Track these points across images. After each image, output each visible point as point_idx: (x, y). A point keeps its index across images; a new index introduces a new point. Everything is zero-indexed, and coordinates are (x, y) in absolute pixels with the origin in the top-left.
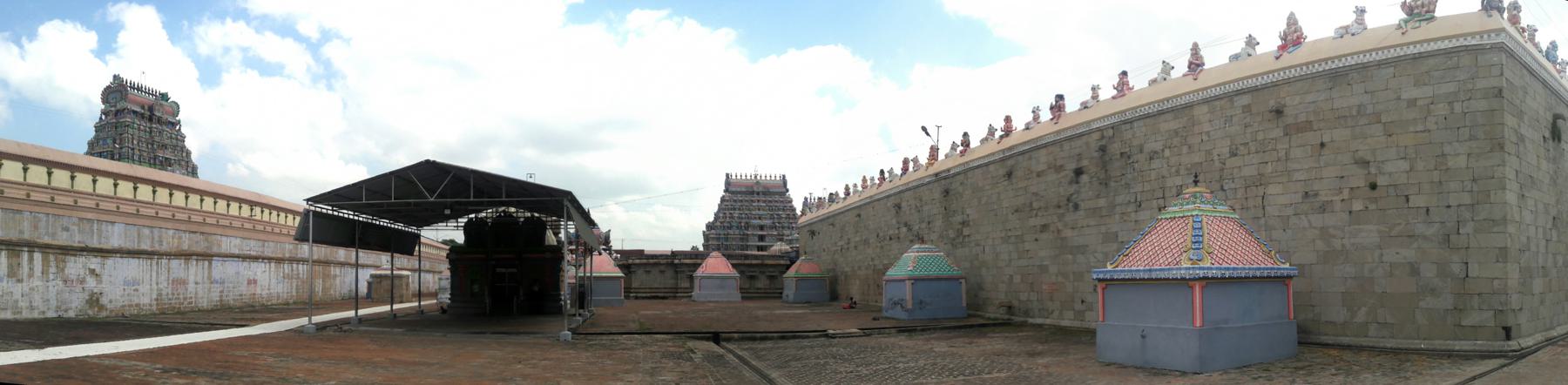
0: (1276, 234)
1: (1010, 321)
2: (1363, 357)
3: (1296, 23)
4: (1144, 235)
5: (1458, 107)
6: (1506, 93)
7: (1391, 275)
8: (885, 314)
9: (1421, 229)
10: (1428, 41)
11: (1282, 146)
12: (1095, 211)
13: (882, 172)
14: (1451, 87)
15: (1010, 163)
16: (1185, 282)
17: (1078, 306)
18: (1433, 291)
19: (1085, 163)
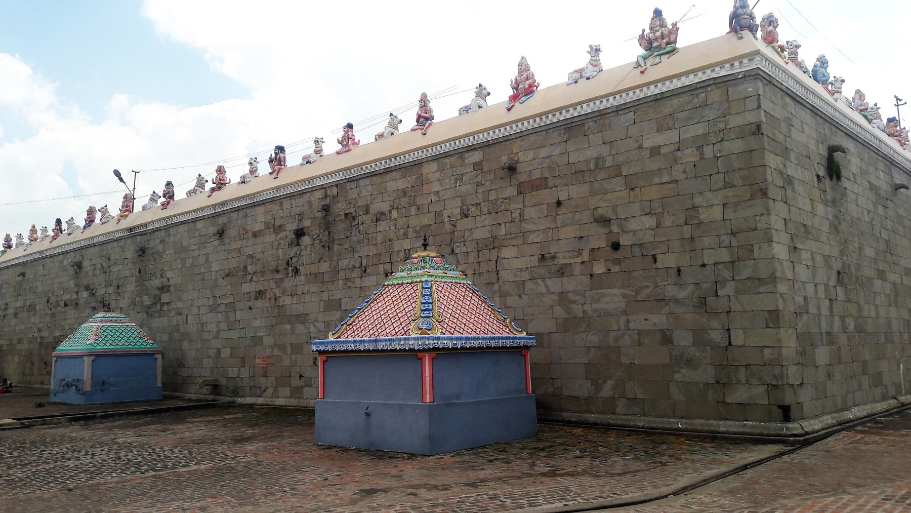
0: (511, 301)
1: (217, 402)
2: (612, 438)
3: (527, 69)
4: (369, 303)
5: (708, 152)
6: (765, 129)
7: (640, 344)
8: (53, 399)
9: (671, 291)
10: (670, 78)
11: (515, 206)
12: (316, 277)
13: (59, 222)
14: (700, 129)
15: (222, 220)
16: (413, 355)
17: (296, 382)
18: (690, 363)
19: (307, 223)
